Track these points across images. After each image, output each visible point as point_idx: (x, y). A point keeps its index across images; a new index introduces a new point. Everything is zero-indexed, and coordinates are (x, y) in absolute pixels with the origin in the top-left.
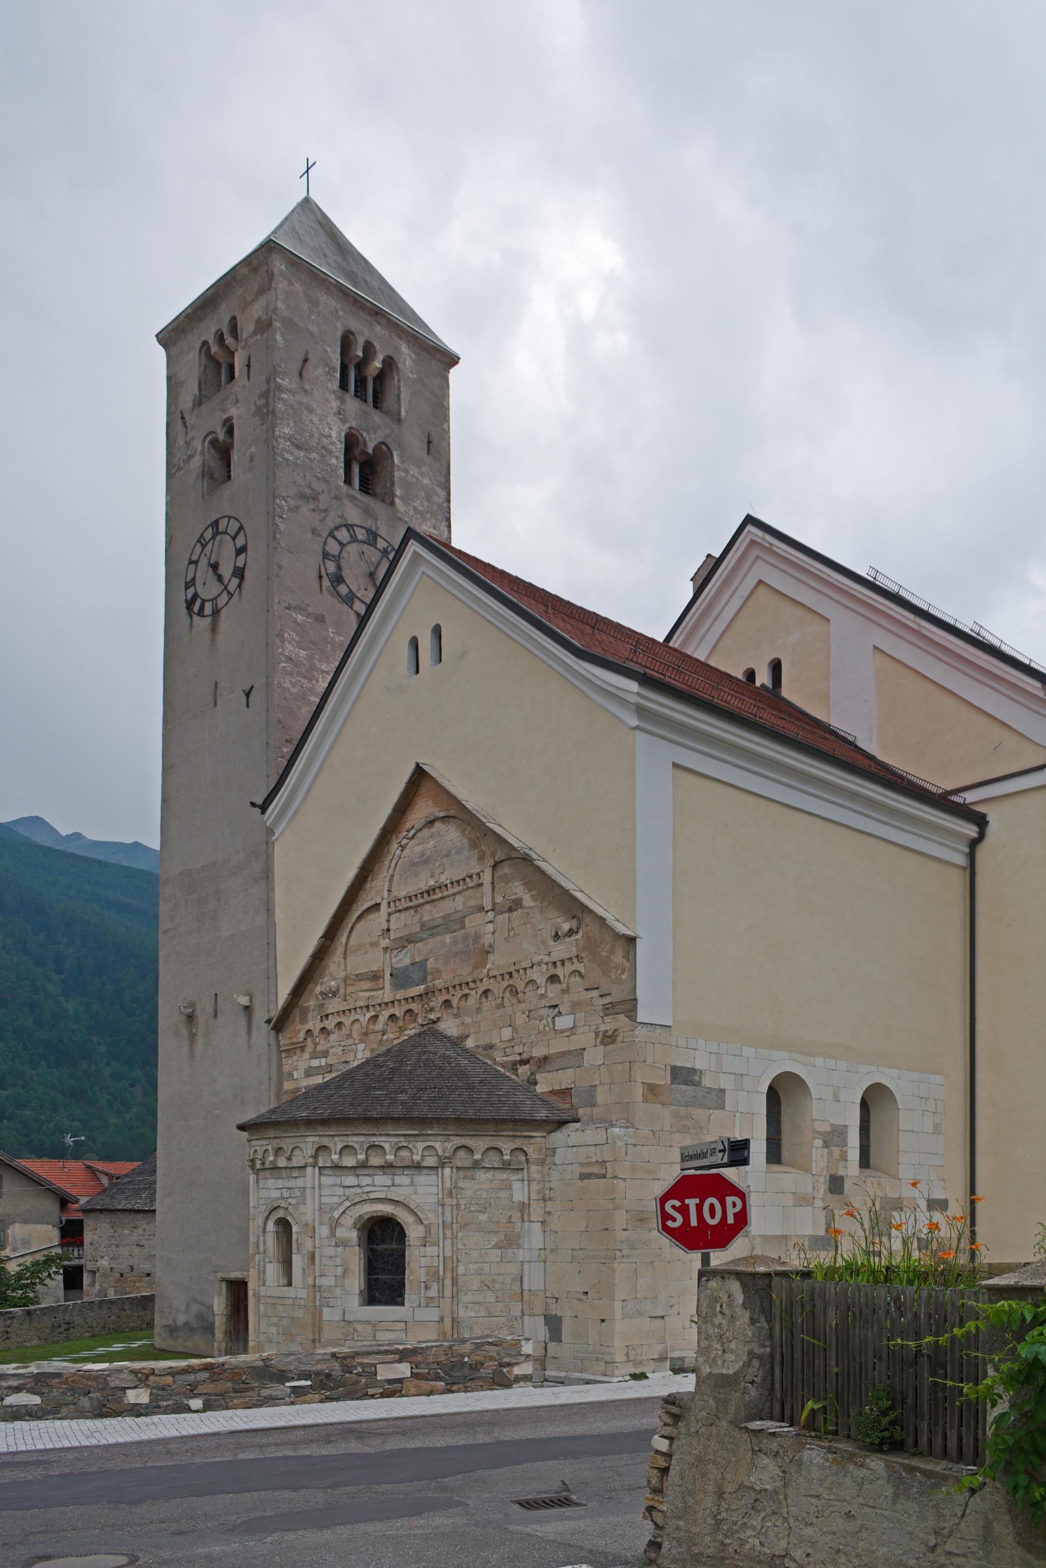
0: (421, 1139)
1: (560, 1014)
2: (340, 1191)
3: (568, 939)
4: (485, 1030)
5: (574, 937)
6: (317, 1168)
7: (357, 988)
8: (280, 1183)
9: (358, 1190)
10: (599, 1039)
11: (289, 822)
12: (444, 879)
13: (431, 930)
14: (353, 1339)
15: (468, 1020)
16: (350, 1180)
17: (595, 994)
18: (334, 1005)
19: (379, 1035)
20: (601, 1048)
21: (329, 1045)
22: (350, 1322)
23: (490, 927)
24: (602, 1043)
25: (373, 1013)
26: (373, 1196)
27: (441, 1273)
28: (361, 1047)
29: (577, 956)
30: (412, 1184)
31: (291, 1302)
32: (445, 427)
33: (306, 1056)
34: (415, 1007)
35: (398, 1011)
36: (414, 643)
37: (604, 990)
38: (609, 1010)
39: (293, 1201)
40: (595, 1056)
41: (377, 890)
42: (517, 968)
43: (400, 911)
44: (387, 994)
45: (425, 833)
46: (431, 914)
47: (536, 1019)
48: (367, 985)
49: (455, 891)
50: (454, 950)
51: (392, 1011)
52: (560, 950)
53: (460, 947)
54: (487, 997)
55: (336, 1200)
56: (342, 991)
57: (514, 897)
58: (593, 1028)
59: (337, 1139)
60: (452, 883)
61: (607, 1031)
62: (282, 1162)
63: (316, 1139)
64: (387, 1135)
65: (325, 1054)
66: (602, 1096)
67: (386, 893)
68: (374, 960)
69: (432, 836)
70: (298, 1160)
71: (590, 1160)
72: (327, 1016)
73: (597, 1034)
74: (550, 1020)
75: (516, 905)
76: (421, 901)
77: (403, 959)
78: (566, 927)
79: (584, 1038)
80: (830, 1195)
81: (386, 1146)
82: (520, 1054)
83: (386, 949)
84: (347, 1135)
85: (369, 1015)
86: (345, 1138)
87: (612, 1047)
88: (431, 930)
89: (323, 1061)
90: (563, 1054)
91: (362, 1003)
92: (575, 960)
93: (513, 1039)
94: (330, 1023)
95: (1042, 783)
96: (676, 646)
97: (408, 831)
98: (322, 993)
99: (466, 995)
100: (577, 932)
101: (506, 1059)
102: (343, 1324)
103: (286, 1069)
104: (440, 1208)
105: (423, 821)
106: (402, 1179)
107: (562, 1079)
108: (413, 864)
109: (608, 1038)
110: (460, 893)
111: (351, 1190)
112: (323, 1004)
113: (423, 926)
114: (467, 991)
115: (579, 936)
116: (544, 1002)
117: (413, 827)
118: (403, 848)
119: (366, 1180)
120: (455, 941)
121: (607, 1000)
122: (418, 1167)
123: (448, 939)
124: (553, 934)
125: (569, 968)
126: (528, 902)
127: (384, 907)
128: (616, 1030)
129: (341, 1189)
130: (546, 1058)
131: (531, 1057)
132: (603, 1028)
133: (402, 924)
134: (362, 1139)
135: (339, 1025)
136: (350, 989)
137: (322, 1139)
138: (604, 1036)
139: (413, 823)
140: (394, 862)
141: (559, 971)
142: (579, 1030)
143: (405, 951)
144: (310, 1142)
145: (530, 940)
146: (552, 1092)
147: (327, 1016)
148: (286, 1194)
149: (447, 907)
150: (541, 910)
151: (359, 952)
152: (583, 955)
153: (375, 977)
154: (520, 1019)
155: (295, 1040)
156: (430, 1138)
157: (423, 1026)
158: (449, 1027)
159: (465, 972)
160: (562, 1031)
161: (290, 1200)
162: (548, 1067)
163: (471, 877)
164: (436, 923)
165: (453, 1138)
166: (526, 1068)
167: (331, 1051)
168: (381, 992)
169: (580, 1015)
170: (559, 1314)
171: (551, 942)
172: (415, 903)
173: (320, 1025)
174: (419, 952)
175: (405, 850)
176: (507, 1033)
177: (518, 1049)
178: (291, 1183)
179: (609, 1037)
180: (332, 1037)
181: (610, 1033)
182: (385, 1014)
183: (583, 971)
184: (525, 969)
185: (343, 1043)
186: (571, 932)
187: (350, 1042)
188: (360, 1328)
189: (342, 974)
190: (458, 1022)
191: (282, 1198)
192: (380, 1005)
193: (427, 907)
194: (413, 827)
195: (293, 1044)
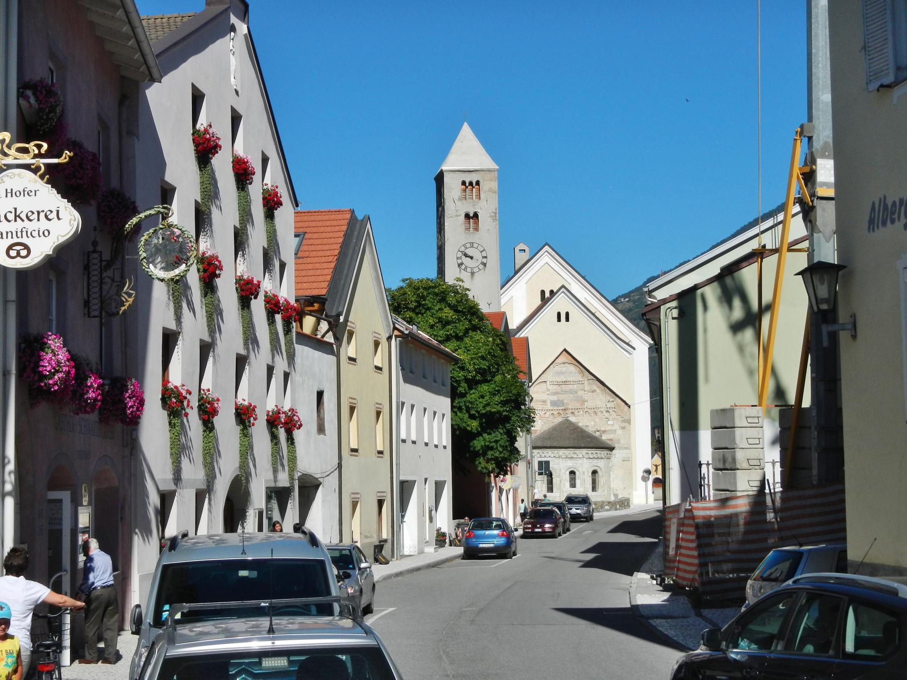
4: (587, 423)
11: (255, 466)
12: (569, 379)
13: (566, 392)
16: (591, 461)
32: (23, 346)
36: (320, 394)
38: (624, 421)
40: (619, 432)
52: (609, 405)
62: (575, 456)
66: (622, 441)
70: (580, 456)
75: (594, 391)
77: (555, 398)
79: (616, 427)
80: (627, 496)
88: (566, 392)
95: (404, 677)
96: (833, 190)
107: (611, 436)
109: (623, 428)
126: (598, 390)
133: (553, 388)
144: (584, 451)
145: (601, 399)
153: (544, 402)
154: (597, 420)
158: (573, 419)
159: (578, 405)
176: (593, 423)
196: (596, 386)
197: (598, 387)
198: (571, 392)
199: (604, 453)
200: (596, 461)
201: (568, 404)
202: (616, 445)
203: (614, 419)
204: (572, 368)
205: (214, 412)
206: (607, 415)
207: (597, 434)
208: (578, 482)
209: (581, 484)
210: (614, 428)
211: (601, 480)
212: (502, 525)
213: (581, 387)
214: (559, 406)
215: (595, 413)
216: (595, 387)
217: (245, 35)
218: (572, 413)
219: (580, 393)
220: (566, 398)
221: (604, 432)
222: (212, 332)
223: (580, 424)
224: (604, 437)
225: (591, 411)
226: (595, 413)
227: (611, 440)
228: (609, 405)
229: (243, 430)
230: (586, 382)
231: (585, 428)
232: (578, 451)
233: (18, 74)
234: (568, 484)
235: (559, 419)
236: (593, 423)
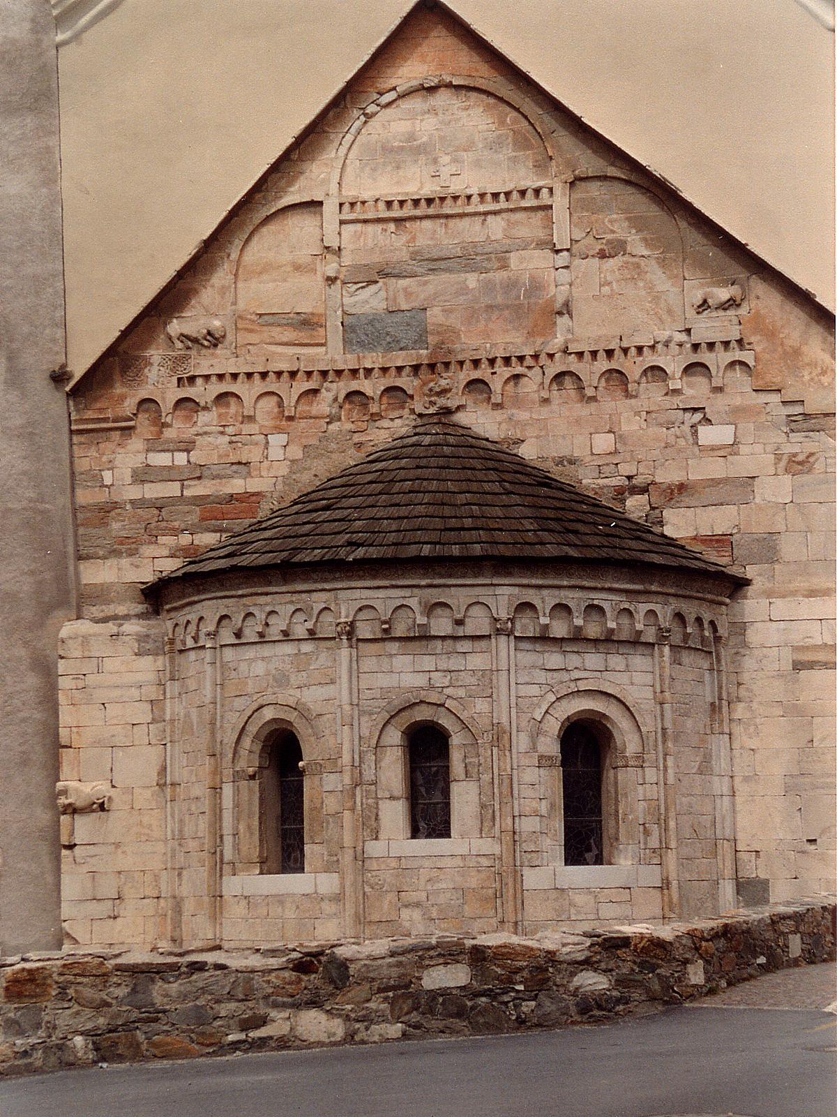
0: (642, 598)
1: (708, 421)
2: (541, 677)
3: (721, 313)
6: (512, 638)
7: (265, 336)
8: (428, 662)
9: (565, 676)
10: (783, 463)
12: (456, 187)
13: (436, 263)
14: (569, 919)
15: (523, 415)
16: (554, 659)
17: (774, 398)
18: (205, 363)
19: (323, 422)
20: (787, 478)
21: (194, 430)
22: (563, 890)
23: (564, 276)
24: (787, 471)
25: (311, 385)
26: (583, 686)
27: (662, 811)
28: (277, 440)
29: (740, 342)
30: (627, 669)
31: (459, 862)
33: (136, 444)
34: (406, 382)
35: (370, 387)
37: (789, 395)
39: (461, 693)
40: (776, 489)
41: (317, 178)
42: (625, 345)
43: (365, 221)
44: (333, 354)
45: (416, 103)
46: (428, 235)
47: (661, 425)
48: (289, 335)
49: (482, 208)
50: (487, 300)
51: (354, 385)
53: (499, 299)
54: (560, 384)
55: (534, 690)
56: (230, 337)
57: (609, 236)
58: (769, 448)
59: (545, 592)
60: (482, 196)
61: (795, 455)
62: (442, 625)
63: (516, 590)
64: (610, 590)
65: (188, 447)
67: (333, 188)
68: (305, 294)
69: (433, 111)
70: (478, 623)
71: (810, 642)
72: (192, 379)
73: (778, 458)
74: (686, 428)
76: (418, 212)
77: (370, 301)
78: (723, 294)
81: (606, 605)
82: (629, 478)
83: (331, 280)
84: (559, 587)
85: (303, 385)
86: (556, 592)
87: (806, 478)
88: (436, 263)
89: (181, 459)
90: (715, 482)
91: (285, 366)
92: (734, 344)
93: (616, 452)
94: (202, 392)
97: (381, 94)
98: (184, 337)
99: (516, 377)
100: (739, 305)
101: (600, 481)
102: (554, 894)
103: (83, 465)
104: (658, 707)
105: (415, 83)
106: (616, 661)
107: (718, 520)
108: (387, 150)
109: (798, 465)
110: (495, 213)
111: (555, 674)
112: (185, 358)
113: (415, 255)
114: (519, 370)
115: (743, 311)
116: (677, 401)
117: (394, 89)
118: (369, 117)
119: (574, 661)
120: (488, 287)
121: (798, 409)
122: (636, 642)
123: (472, 280)
125: (258, 386)
127: (330, 208)
128: (812, 454)
129: (543, 673)
130: (682, 487)
131: (653, 483)
132: (788, 449)
134: (578, 594)
135: (222, 397)
136: (244, 338)
137: (524, 591)
138: (790, 461)
139: (399, 82)
140: (349, 137)
141: (705, 357)
142: (744, 449)
143: (373, 288)
144: (502, 596)
146: (694, 538)
147: (192, 379)
148: (439, 680)
149: (470, 231)
150: (662, 263)
151: (265, 277)
152: (752, 339)
153: (307, 323)
154: (631, 425)
155: (109, 414)
156: (654, 598)
157: (420, 415)
158: (481, 421)
160: (713, 448)
161: (447, 691)
162: (687, 500)
163: (523, 193)
164: (442, 254)
165: (671, 600)
166: (642, 499)
167: (200, 441)
168: (324, 349)
169: (747, 427)
170: (762, 876)
171: (691, 313)
172: (396, 213)
173: (175, 393)
174: (408, 294)
175: (389, 124)
176: (604, 442)
177: (626, 469)
178: (455, 663)
179: (800, 463)
180: (203, 417)
181: (800, 458)
182: (342, 387)
183: (751, 363)
184: (640, 349)
185: (230, 430)
186: (732, 303)
187: (247, 428)
188: (580, 899)
189: (229, 309)
190: (499, 415)
191: (432, 687)
192: (324, 374)
193: (427, 224)
194: (394, 89)
195: (105, 420)
196: (618, 215)
197: (638, 223)
198: (468, 260)
199: (653, 611)
200: (593, 660)
202: (750, 572)
203: (736, 415)
204: (474, 120)
205: (800, 663)
206: (697, 390)
207: (635, 506)
208: (464, 799)
209: (487, 815)
210: (741, 466)
211: (633, 790)
213: (530, 227)
214: (394, 345)
215: (617, 377)
216: (616, 225)
217: (122, 435)
218: (477, 385)
220: (443, 300)
223: (528, 452)
224: (679, 524)
226: (617, 377)
227: (722, 541)
228: (709, 327)
229: (142, 613)
230: (560, 202)
231: (556, 472)
232: (459, 595)
233: (256, 184)
234: (395, 814)
235: (392, 428)
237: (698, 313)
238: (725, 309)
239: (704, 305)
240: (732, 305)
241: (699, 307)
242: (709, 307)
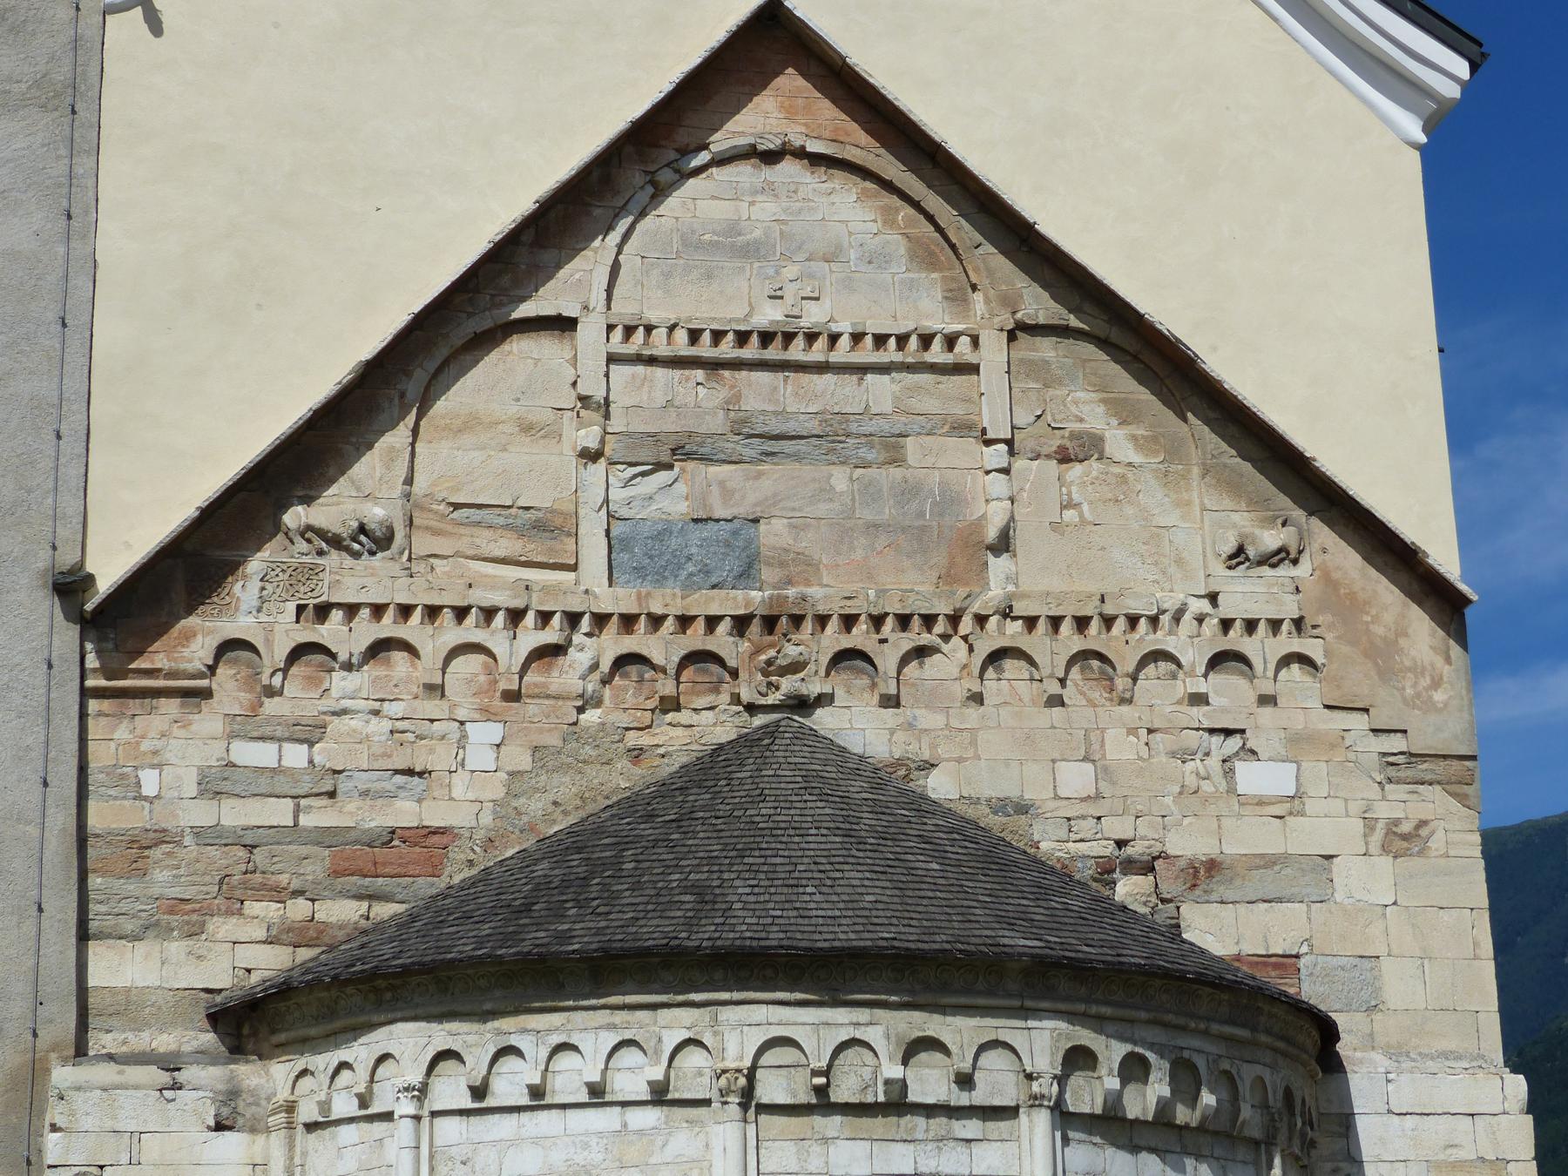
3: (1266, 571)
5: (1285, 571)
13: (772, 442)
52: (1248, 594)
62: (930, 1082)
70: (997, 1082)
77: (665, 498)
78: (1271, 539)
88: (772, 442)
100: (1295, 562)
124: (1229, 547)
126: (1119, 443)
153: (548, 529)
154: (1121, 748)
158: (856, 724)
159: (915, 585)
176: (1076, 778)
198: (832, 438)
201: (800, 566)
203: (1298, 745)
204: (846, 210)
210: (1304, 836)
212: (1417, 670)
213: (937, 396)
219: (938, 460)
221: (1205, 873)
222: (92, 1089)
225: (1052, 650)
228: (1248, 594)
230: (993, 353)
236: (1076, 778)
237: (1230, 568)
238: (1273, 566)
239: (1238, 556)
240: (1282, 560)
241: (1231, 557)
242: (1247, 559)
